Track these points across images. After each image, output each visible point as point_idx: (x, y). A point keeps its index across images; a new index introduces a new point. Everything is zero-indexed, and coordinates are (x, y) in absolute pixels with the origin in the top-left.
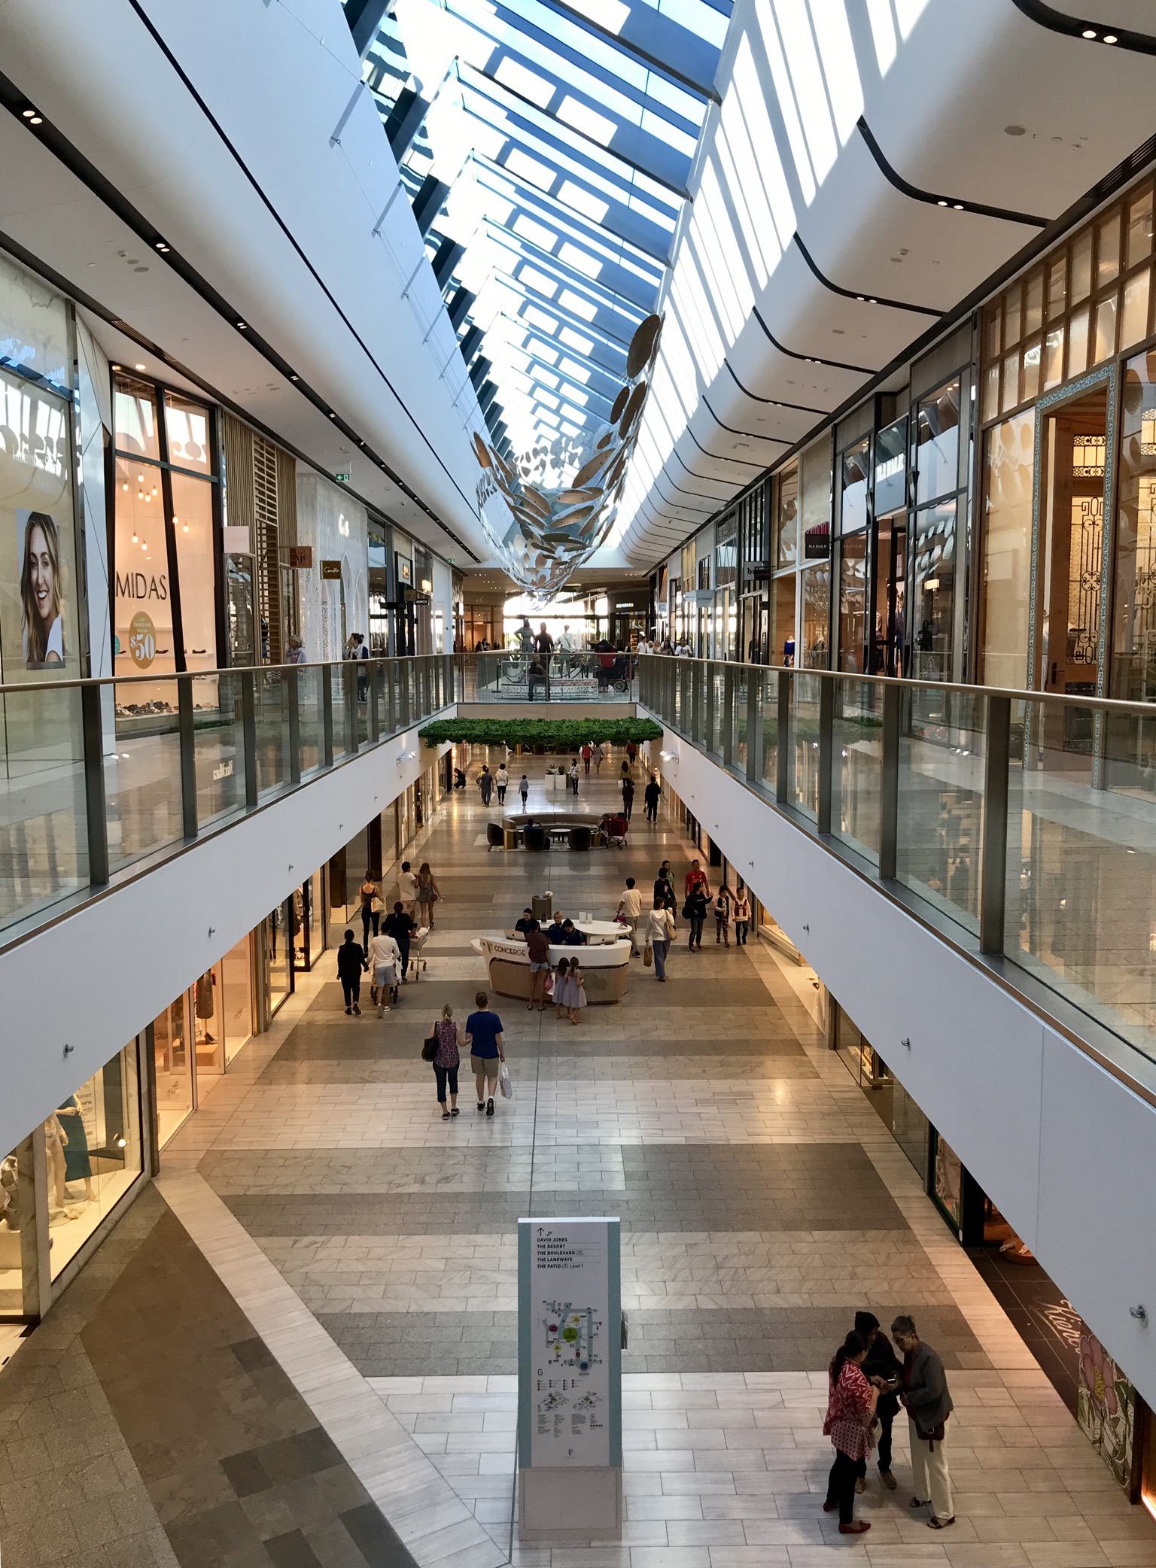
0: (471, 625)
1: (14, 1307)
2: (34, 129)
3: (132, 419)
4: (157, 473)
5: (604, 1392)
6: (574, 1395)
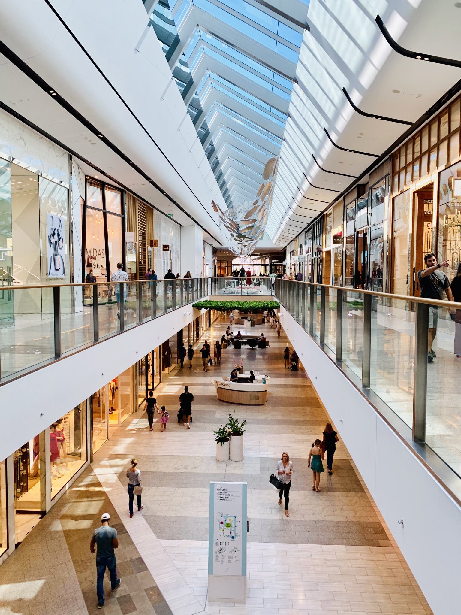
0: (220, 268)
1: (38, 508)
2: (53, 97)
3: (94, 196)
4: (101, 213)
5: (240, 548)
6: (229, 548)
